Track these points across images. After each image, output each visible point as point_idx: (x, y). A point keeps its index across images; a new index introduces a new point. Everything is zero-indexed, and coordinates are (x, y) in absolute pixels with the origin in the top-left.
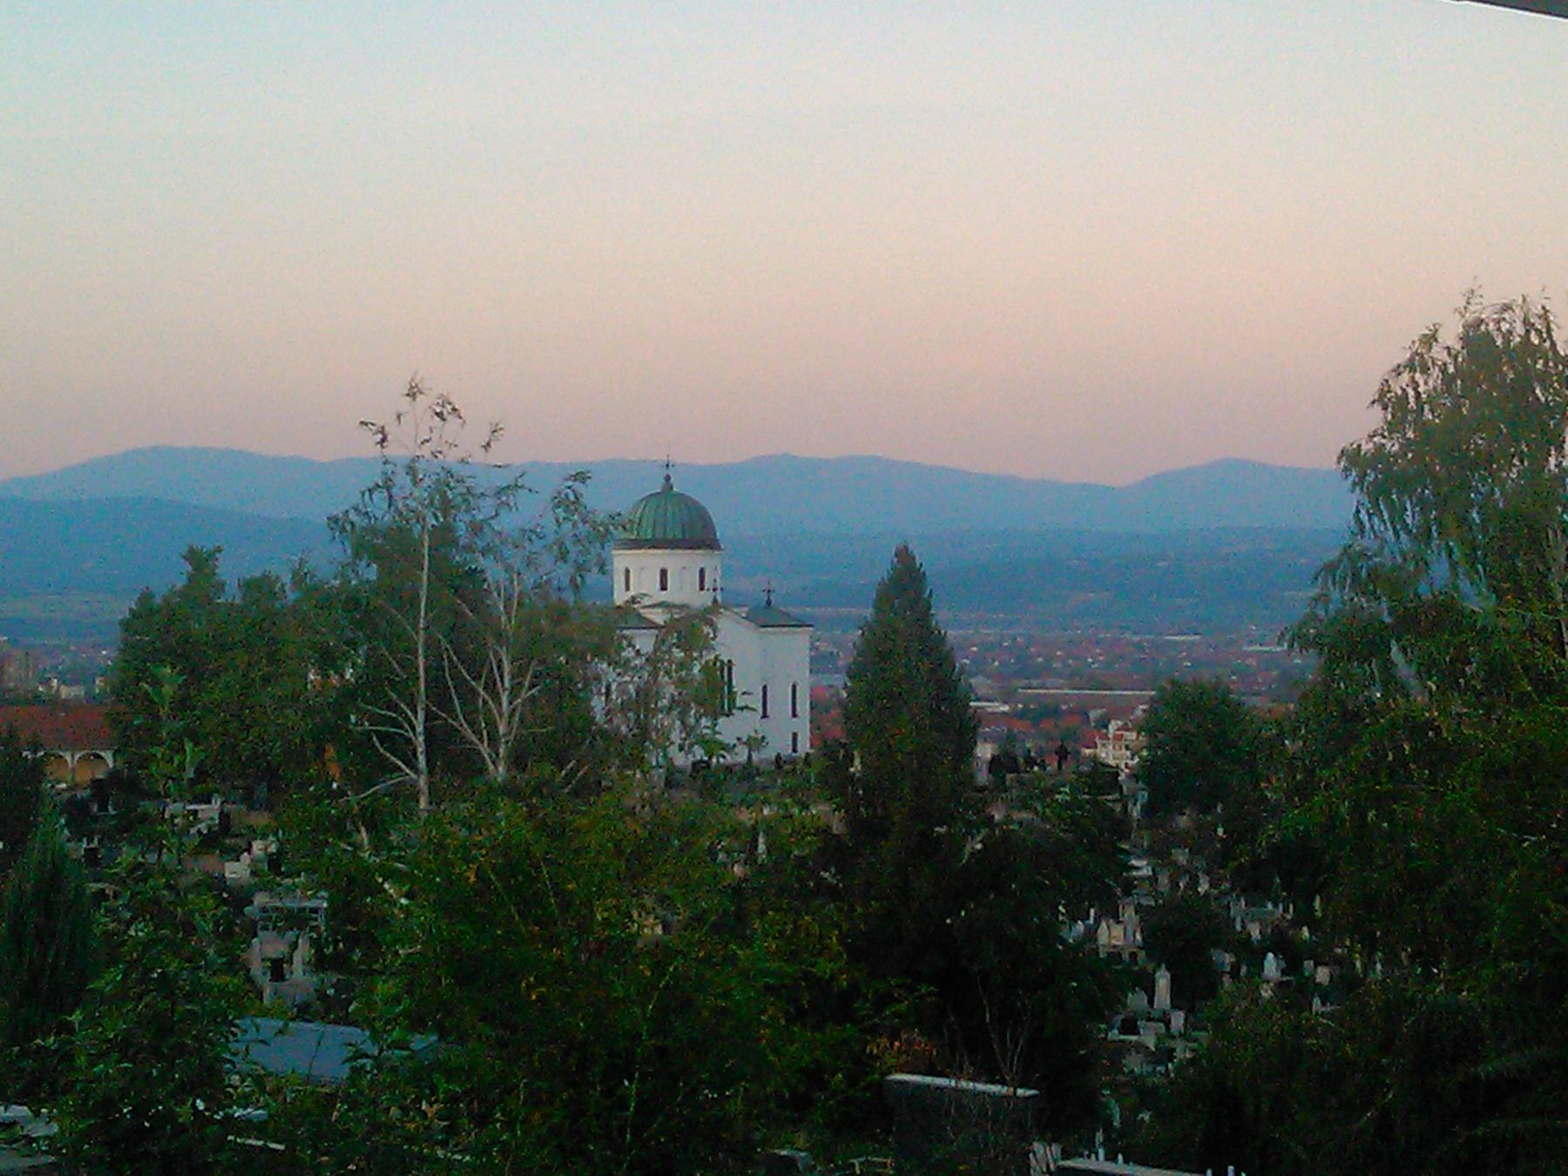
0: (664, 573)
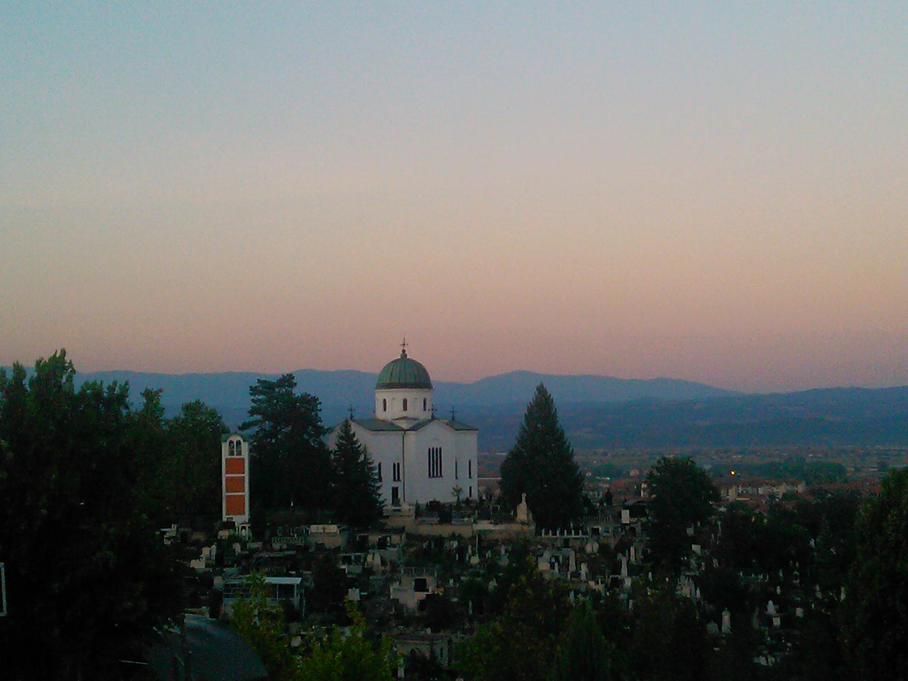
0: (405, 401)
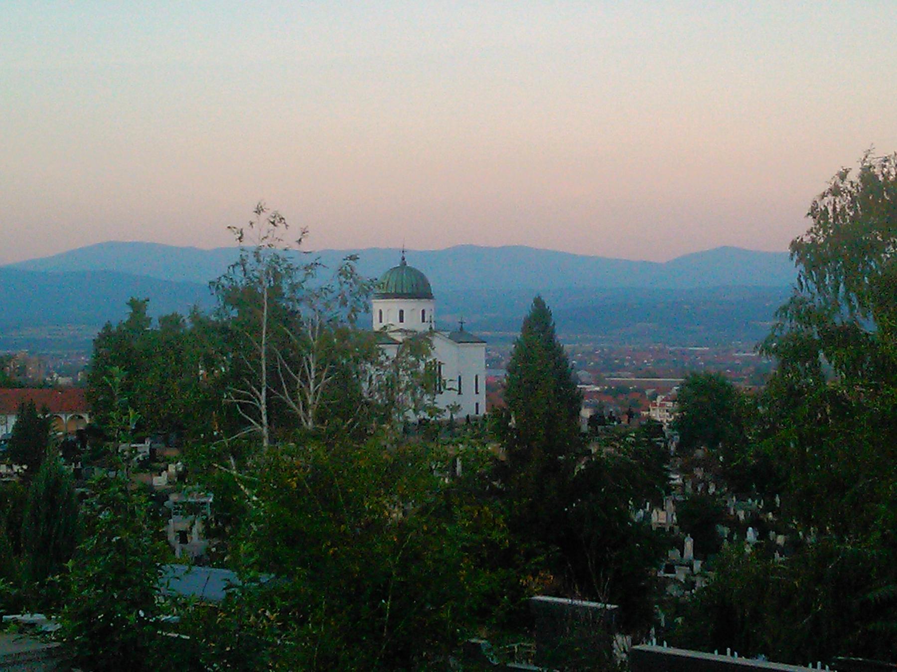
0: (401, 312)
